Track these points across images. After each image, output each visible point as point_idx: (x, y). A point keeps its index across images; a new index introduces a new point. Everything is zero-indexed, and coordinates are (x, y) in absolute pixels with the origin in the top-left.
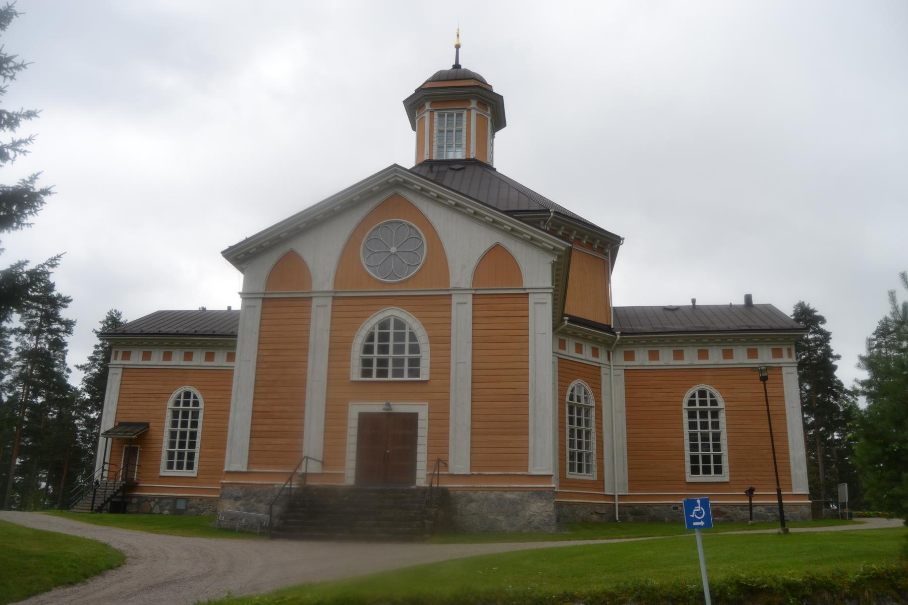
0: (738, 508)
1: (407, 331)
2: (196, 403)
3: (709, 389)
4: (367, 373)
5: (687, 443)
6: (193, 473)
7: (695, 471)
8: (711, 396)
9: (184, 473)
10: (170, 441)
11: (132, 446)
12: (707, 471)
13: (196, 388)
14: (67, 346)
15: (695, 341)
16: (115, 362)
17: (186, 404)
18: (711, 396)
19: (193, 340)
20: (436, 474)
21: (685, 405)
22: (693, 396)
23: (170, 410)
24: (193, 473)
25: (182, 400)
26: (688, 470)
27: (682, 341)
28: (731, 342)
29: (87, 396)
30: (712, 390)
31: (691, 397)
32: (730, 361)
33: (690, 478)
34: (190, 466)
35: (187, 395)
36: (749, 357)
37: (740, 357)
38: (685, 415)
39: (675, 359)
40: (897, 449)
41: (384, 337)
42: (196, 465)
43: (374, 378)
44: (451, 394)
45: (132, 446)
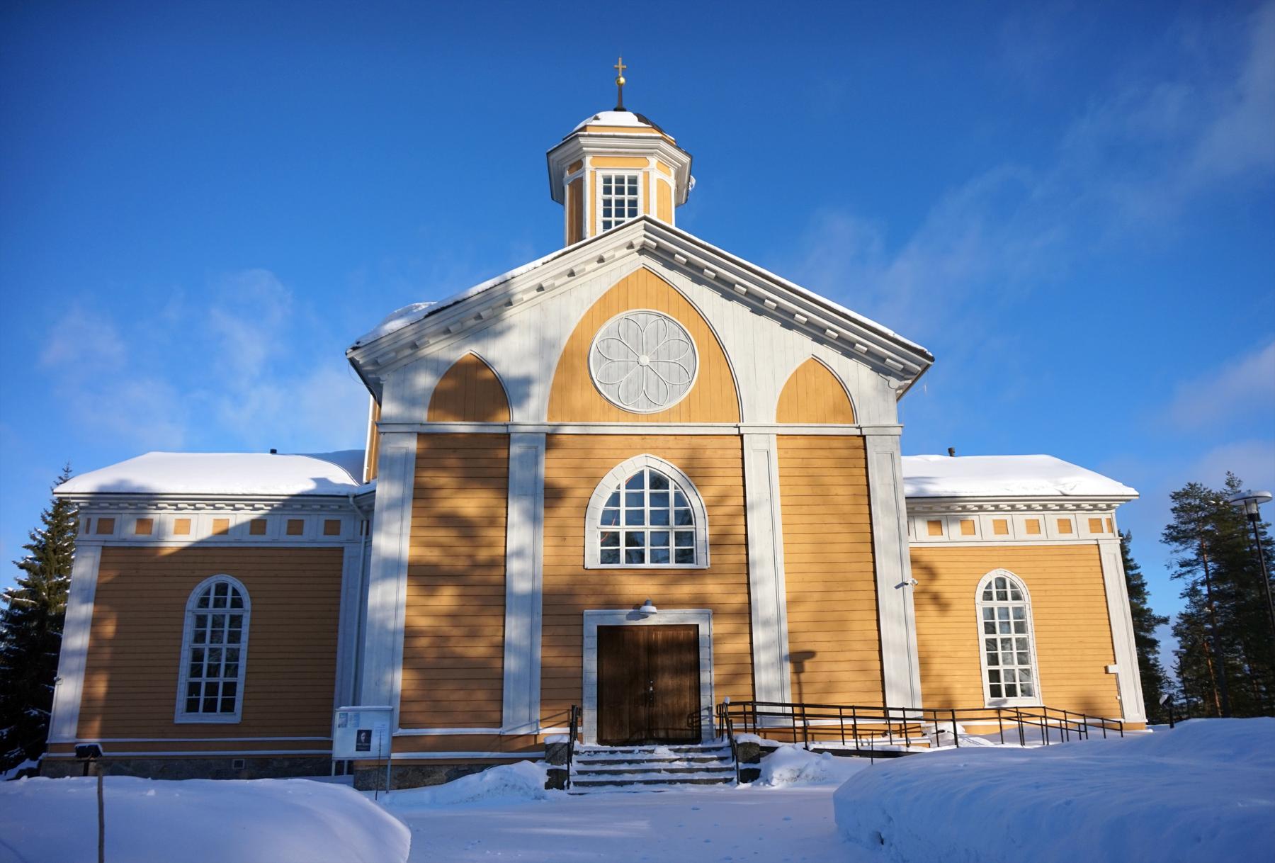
1: (672, 491)
2: (237, 603)
3: (1010, 576)
5: (1032, 651)
6: (234, 718)
8: (1012, 586)
9: (217, 718)
10: (192, 665)
13: (240, 580)
16: (86, 537)
17: (219, 603)
18: (1012, 586)
20: (749, 713)
22: (989, 586)
23: (190, 614)
24: (234, 718)
25: (212, 597)
27: (319, 507)
28: (297, 509)
29: (1249, 673)
31: (986, 588)
34: (228, 706)
35: (1001, 582)
37: (1050, 532)
40: (1242, 649)
41: (637, 499)
42: (238, 705)
43: (672, 564)
44: (99, 561)
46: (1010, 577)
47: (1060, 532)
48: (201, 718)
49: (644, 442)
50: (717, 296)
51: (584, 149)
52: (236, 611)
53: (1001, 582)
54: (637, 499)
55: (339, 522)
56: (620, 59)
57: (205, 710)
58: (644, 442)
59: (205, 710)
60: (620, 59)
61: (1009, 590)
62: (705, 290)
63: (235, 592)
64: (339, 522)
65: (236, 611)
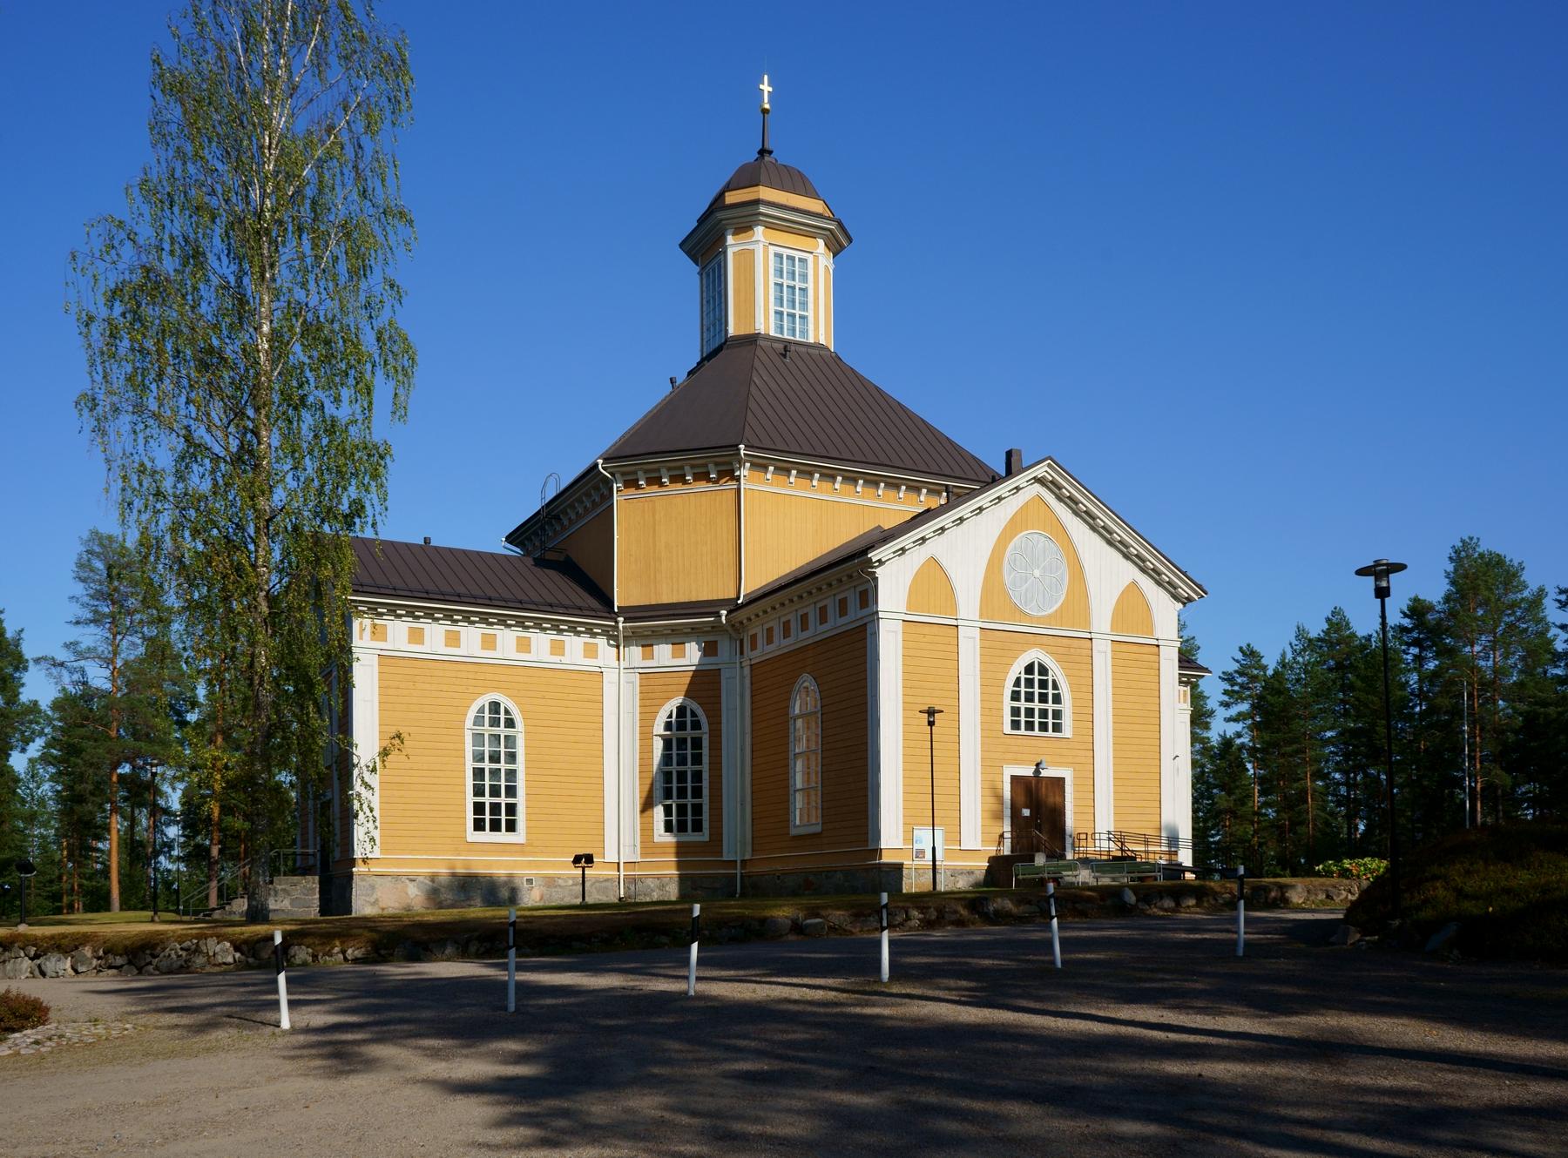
0: (404, 878)
4: (1015, 725)
7: (479, 825)
8: (507, 712)
9: (503, 836)
11: (1052, 901)
12: (495, 827)
14: (1337, 623)
15: (583, 629)
18: (507, 712)
19: (1325, 912)
21: (469, 723)
26: (470, 824)
30: (508, 704)
32: (556, 659)
33: (473, 836)
35: (495, 707)
36: (1012, 729)
38: (469, 739)
39: (1012, 729)
42: (706, 825)
45: (1052, 901)
46: (505, 702)
47: (518, 651)
48: (487, 836)
49: (1035, 639)
50: (1085, 528)
51: (763, 209)
52: (696, 733)
53: (495, 707)
54: (1030, 683)
55: (716, 642)
56: (766, 77)
57: (693, 831)
58: (1035, 639)
59: (693, 831)
60: (766, 77)
61: (502, 716)
62: (1077, 521)
63: (693, 714)
64: (716, 642)
65: (696, 733)
